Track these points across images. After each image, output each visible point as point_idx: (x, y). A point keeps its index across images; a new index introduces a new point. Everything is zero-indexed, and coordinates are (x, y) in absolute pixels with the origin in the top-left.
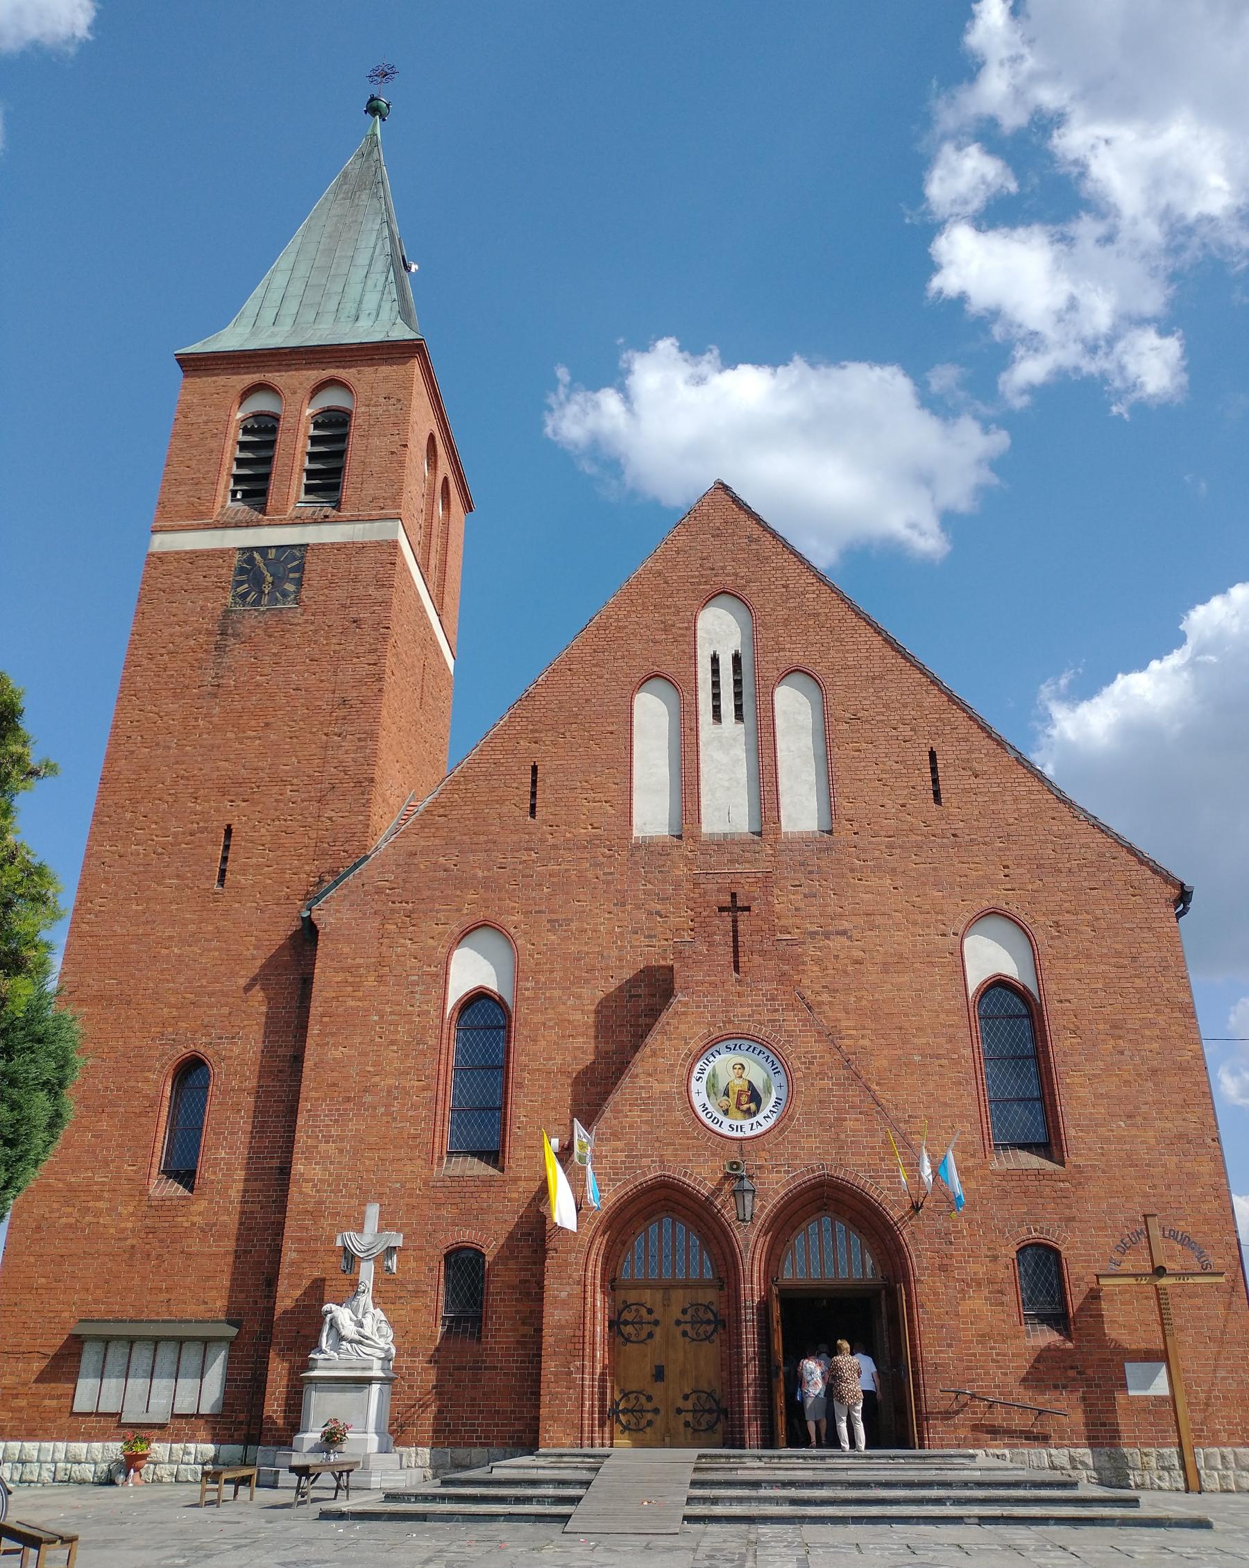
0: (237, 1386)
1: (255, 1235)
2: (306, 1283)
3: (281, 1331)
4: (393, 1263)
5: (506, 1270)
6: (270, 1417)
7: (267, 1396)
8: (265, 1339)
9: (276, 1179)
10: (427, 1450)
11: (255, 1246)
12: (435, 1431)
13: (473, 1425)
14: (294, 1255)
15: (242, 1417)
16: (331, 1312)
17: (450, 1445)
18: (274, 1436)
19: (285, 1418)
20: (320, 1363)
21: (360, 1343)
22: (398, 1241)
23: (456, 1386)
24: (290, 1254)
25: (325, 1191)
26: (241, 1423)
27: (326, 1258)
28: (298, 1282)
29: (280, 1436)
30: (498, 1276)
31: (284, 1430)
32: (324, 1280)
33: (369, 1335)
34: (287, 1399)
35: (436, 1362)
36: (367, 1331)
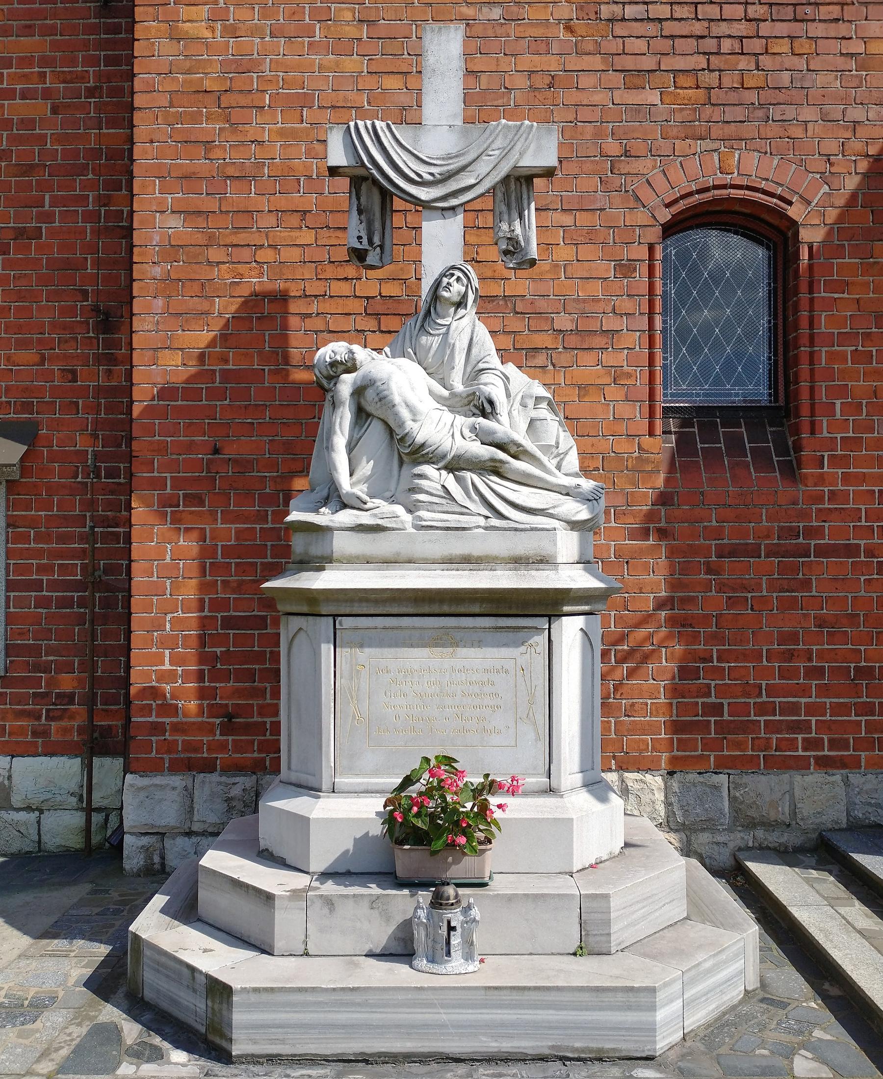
0: (43, 602)
1: (43, 186)
2: (225, 307)
3: (162, 449)
4: (528, 228)
5: (867, 269)
6: (154, 693)
7: (138, 634)
8: (112, 473)
9: (91, 29)
10: (655, 781)
11: (48, 217)
12: (676, 727)
13: (794, 709)
14: (175, 223)
15: (67, 683)
16: (351, 367)
17: (723, 765)
18: (170, 747)
19: (202, 694)
20: (342, 543)
21: (495, 469)
22: (540, 150)
23: (732, 602)
24: (159, 222)
25: (256, 31)
26: (70, 698)
27: (281, 235)
28: (205, 306)
29: (189, 747)
30: (842, 286)
31: (201, 728)
32: (281, 299)
33: (520, 436)
34: (202, 640)
35: (662, 533)
36: (510, 424)
